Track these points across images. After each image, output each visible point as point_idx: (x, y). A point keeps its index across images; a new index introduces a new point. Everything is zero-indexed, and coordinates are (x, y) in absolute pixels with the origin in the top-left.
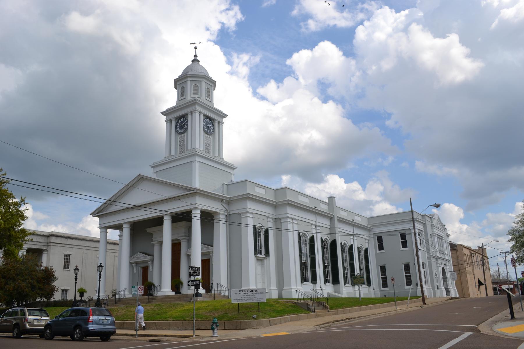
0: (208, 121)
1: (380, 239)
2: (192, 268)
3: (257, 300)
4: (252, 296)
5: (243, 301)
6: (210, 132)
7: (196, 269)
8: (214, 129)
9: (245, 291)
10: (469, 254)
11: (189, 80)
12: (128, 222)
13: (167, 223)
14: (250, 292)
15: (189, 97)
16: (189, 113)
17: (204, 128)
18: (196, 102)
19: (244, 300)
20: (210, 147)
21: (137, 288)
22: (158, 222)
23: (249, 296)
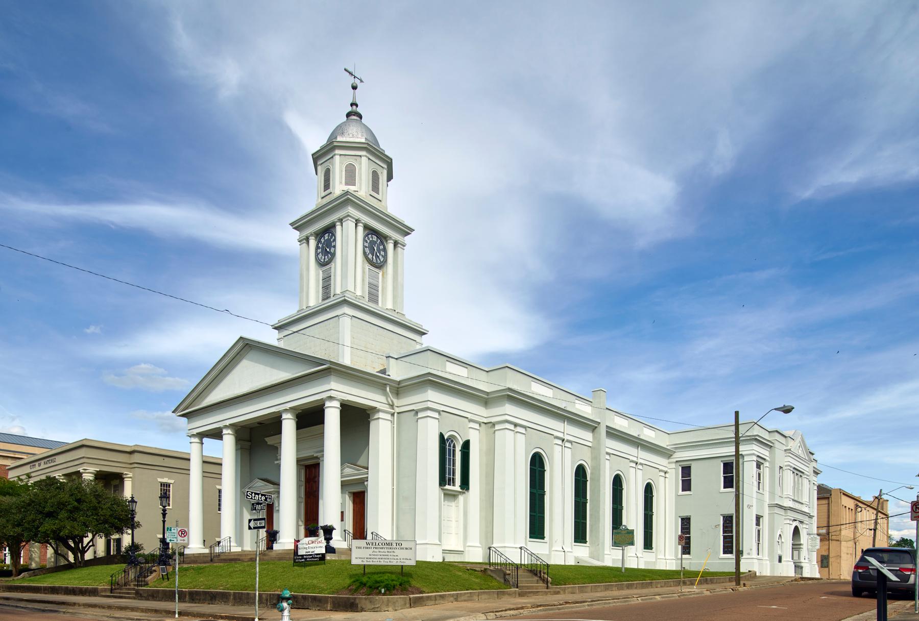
0: (375, 238)
1: (686, 471)
2: (253, 495)
3: (399, 561)
4: (389, 554)
5: (372, 561)
6: (379, 262)
7: (263, 498)
8: (385, 257)
9: (377, 544)
10: (852, 507)
11: (337, 154)
12: (231, 425)
13: (289, 426)
14: (387, 546)
15: (339, 187)
16: (336, 222)
17: (364, 253)
18: (348, 199)
19: (374, 560)
20: (378, 291)
21: (175, 531)
22: (273, 425)
23: (383, 554)
